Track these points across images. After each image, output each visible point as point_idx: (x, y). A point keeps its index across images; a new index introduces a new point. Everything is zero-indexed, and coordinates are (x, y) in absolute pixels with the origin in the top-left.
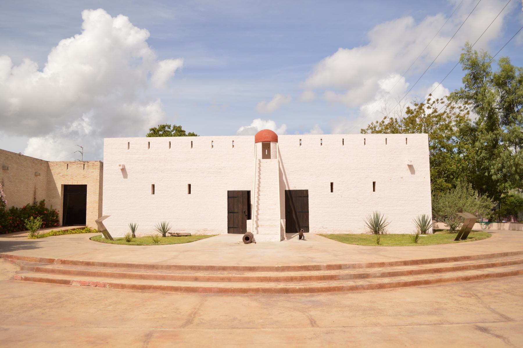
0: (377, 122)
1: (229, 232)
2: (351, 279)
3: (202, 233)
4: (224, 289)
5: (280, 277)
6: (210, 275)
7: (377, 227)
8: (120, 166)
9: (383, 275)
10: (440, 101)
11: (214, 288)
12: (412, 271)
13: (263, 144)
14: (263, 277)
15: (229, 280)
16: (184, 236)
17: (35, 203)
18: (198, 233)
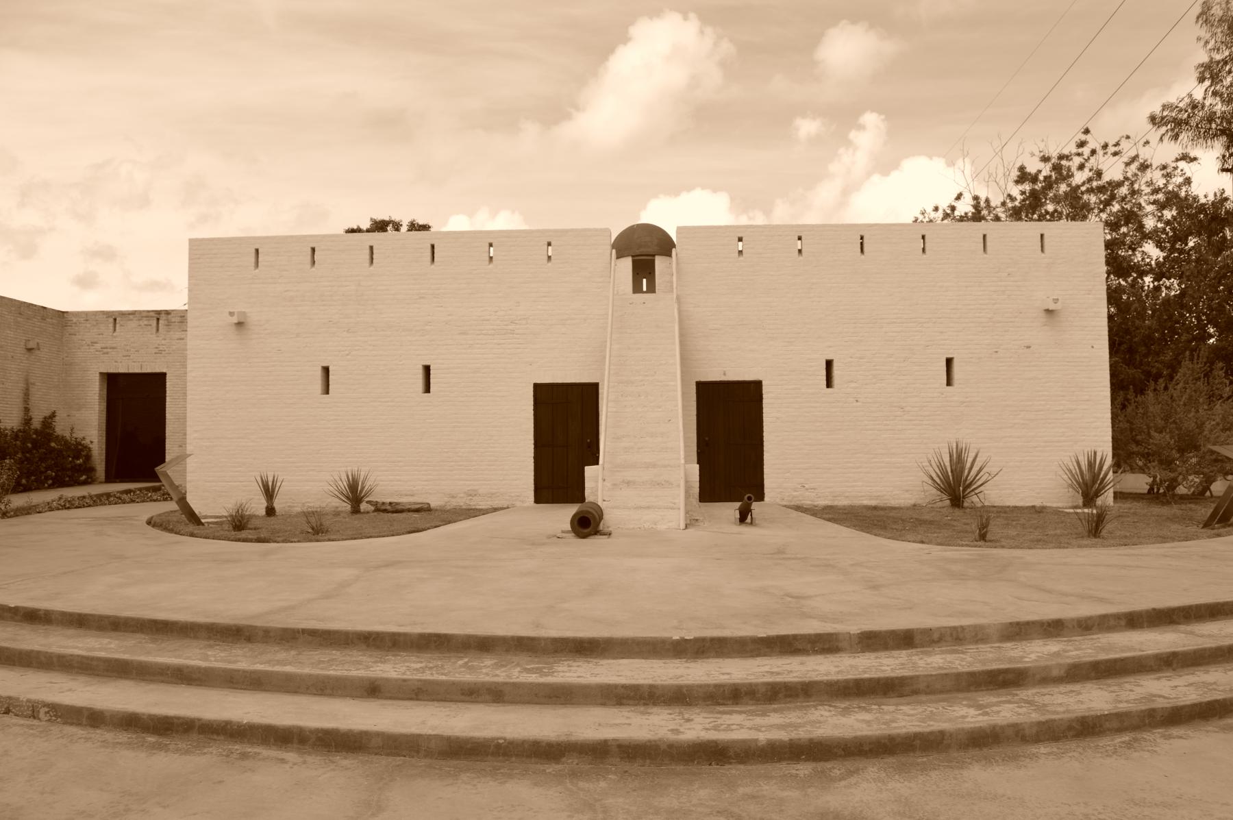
0: (936, 209)
1: (537, 501)
2: (959, 690)
3: (461, 502)
4: (467, 741)
5: (690, 688)
6: (427, 676)
7: (956, 485)
8: (231, 314)
9: (1079, 673)
10: (1111, 149)
11: (429, 738)
12: (1175, 654)
13: (634, 262)
14: (624, 687)
15: (497, 695)
16: (409, 510)
17: (27, 421)
18: (454, 503)
